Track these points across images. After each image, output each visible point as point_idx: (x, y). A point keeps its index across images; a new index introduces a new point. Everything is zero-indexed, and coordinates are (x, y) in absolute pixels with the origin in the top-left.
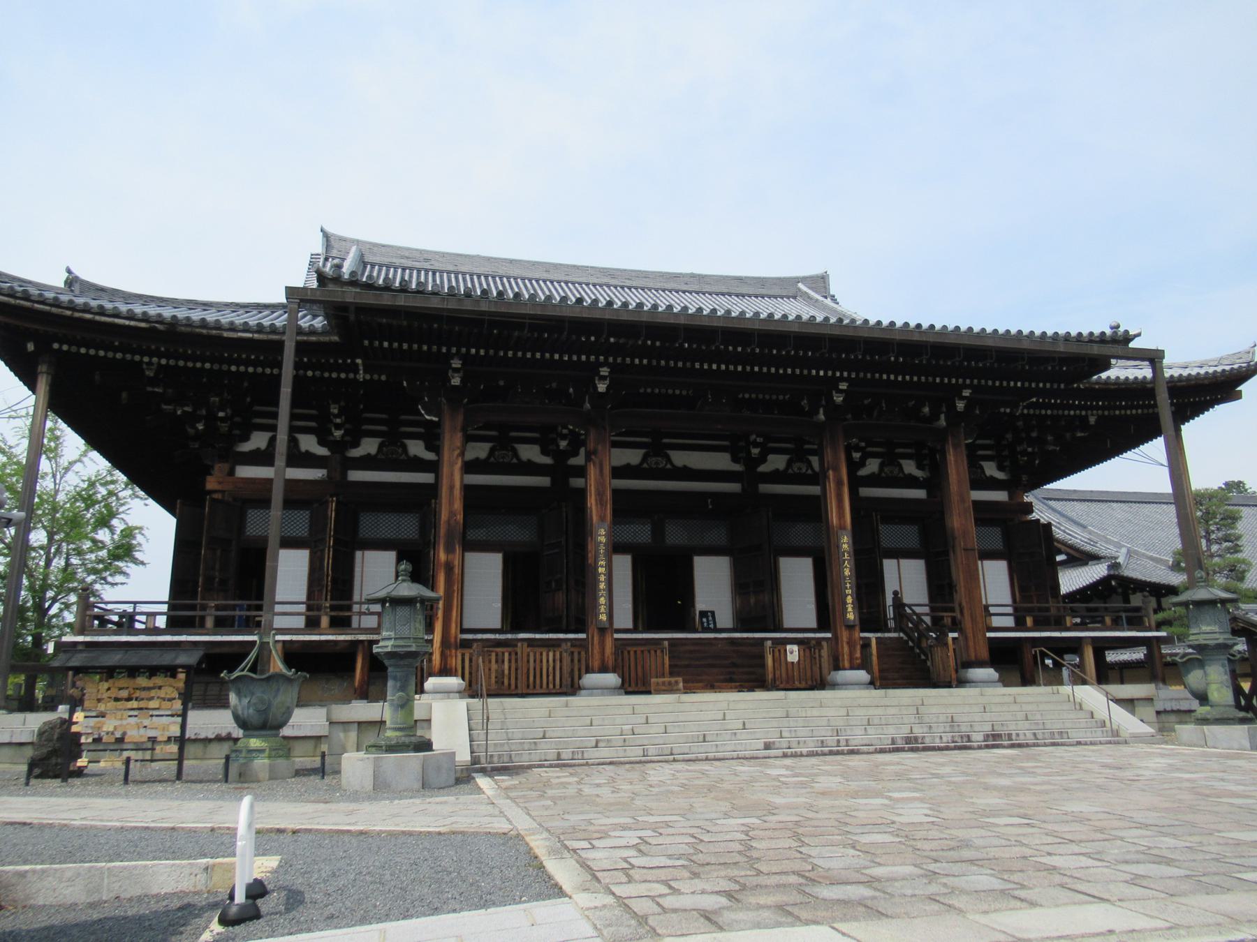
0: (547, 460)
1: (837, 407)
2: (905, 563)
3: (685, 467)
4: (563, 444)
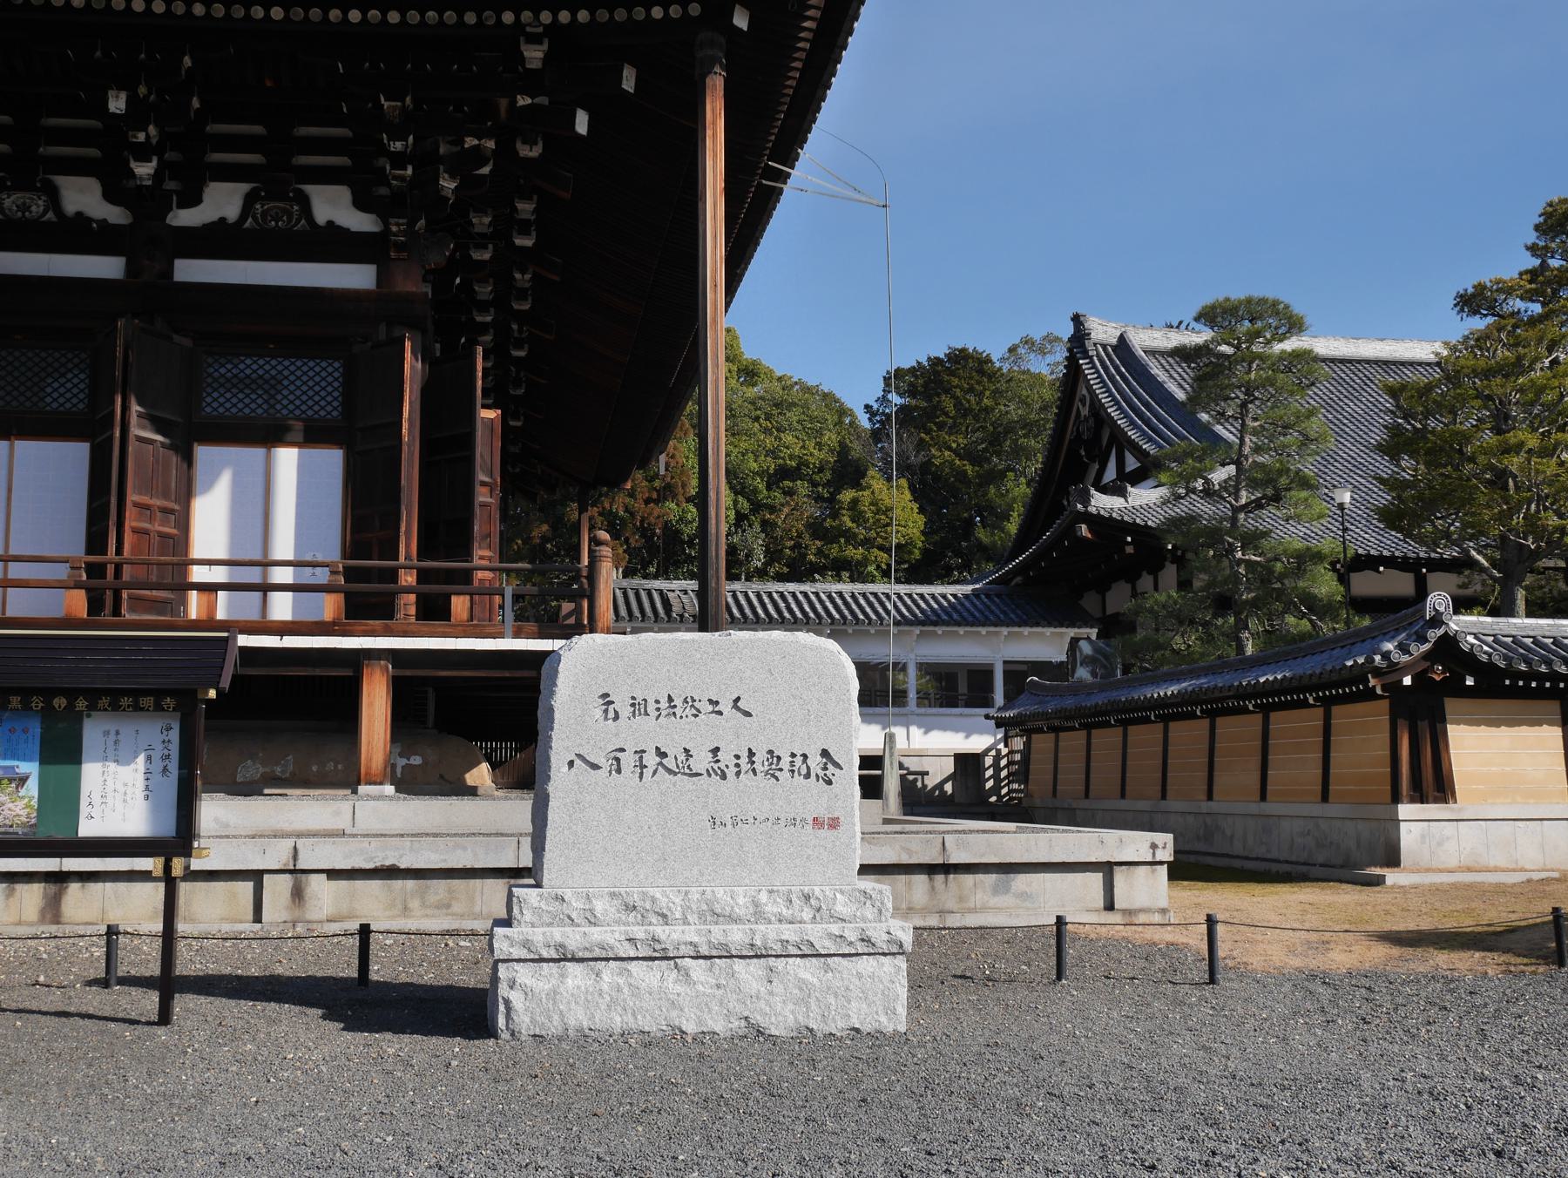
2: (29, 450)
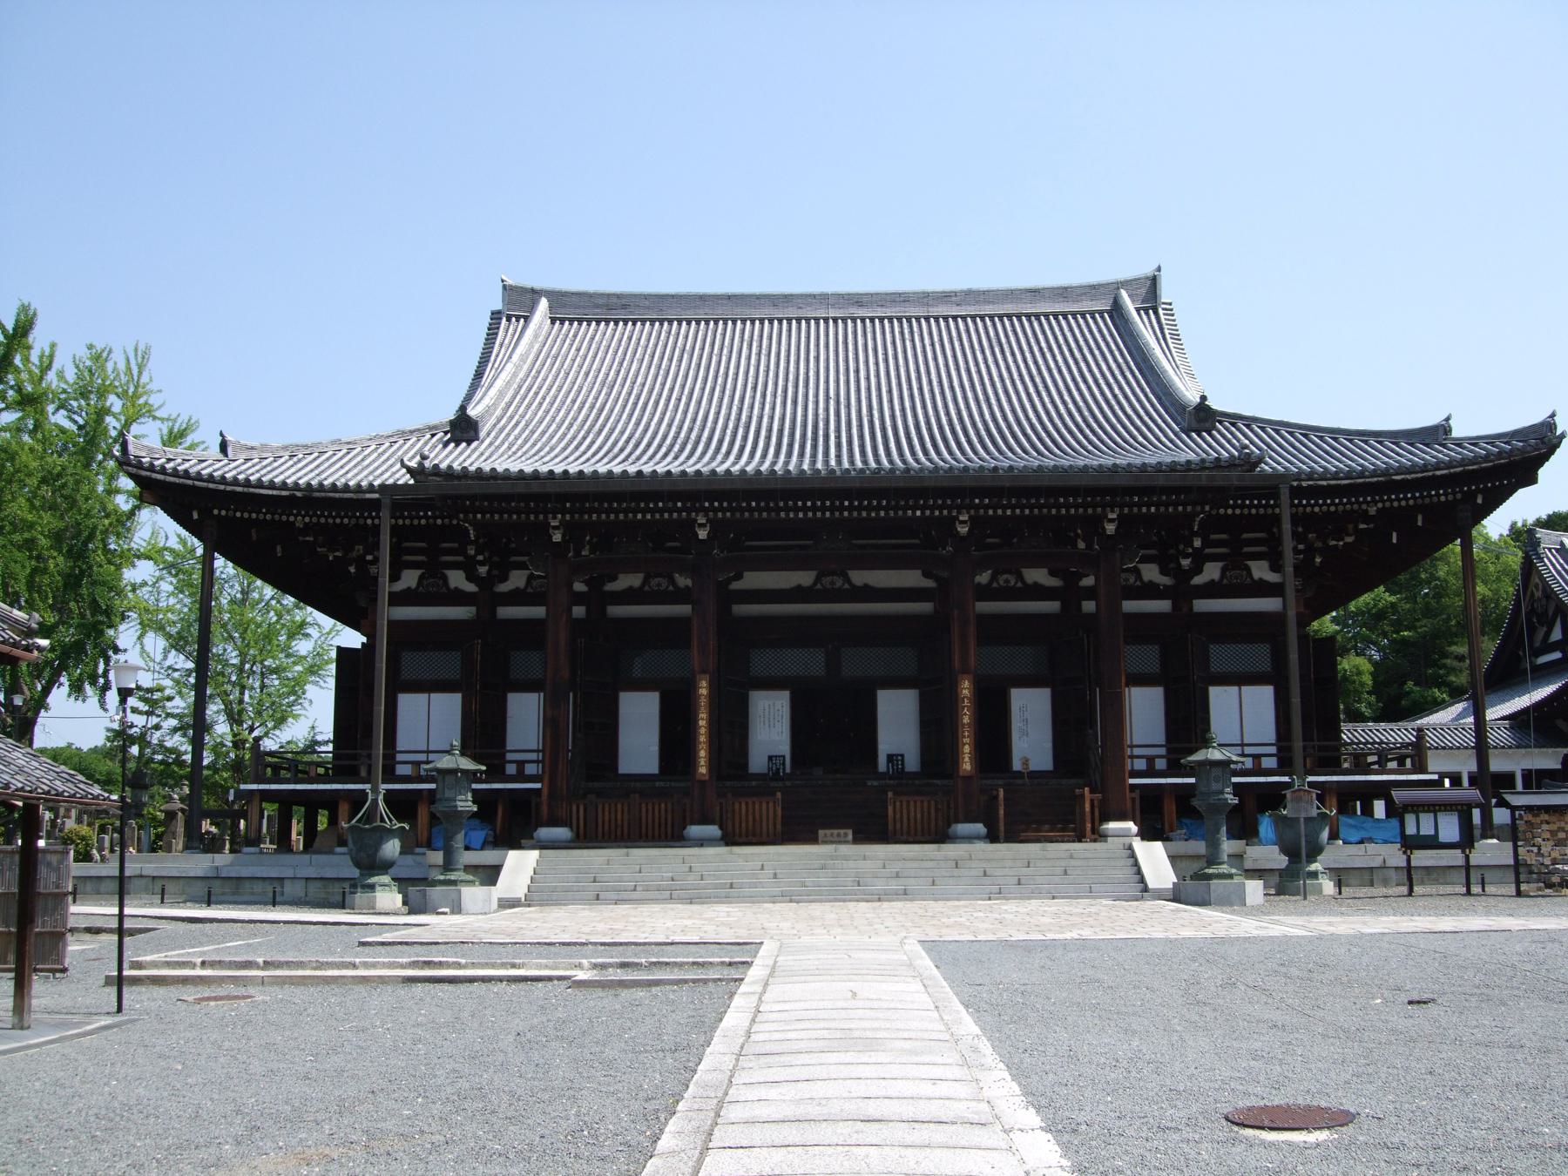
0: (1166, 581)
1: (963, 539)
2: (437, 698)
3: (866, 586)
4: (1186, 562)
